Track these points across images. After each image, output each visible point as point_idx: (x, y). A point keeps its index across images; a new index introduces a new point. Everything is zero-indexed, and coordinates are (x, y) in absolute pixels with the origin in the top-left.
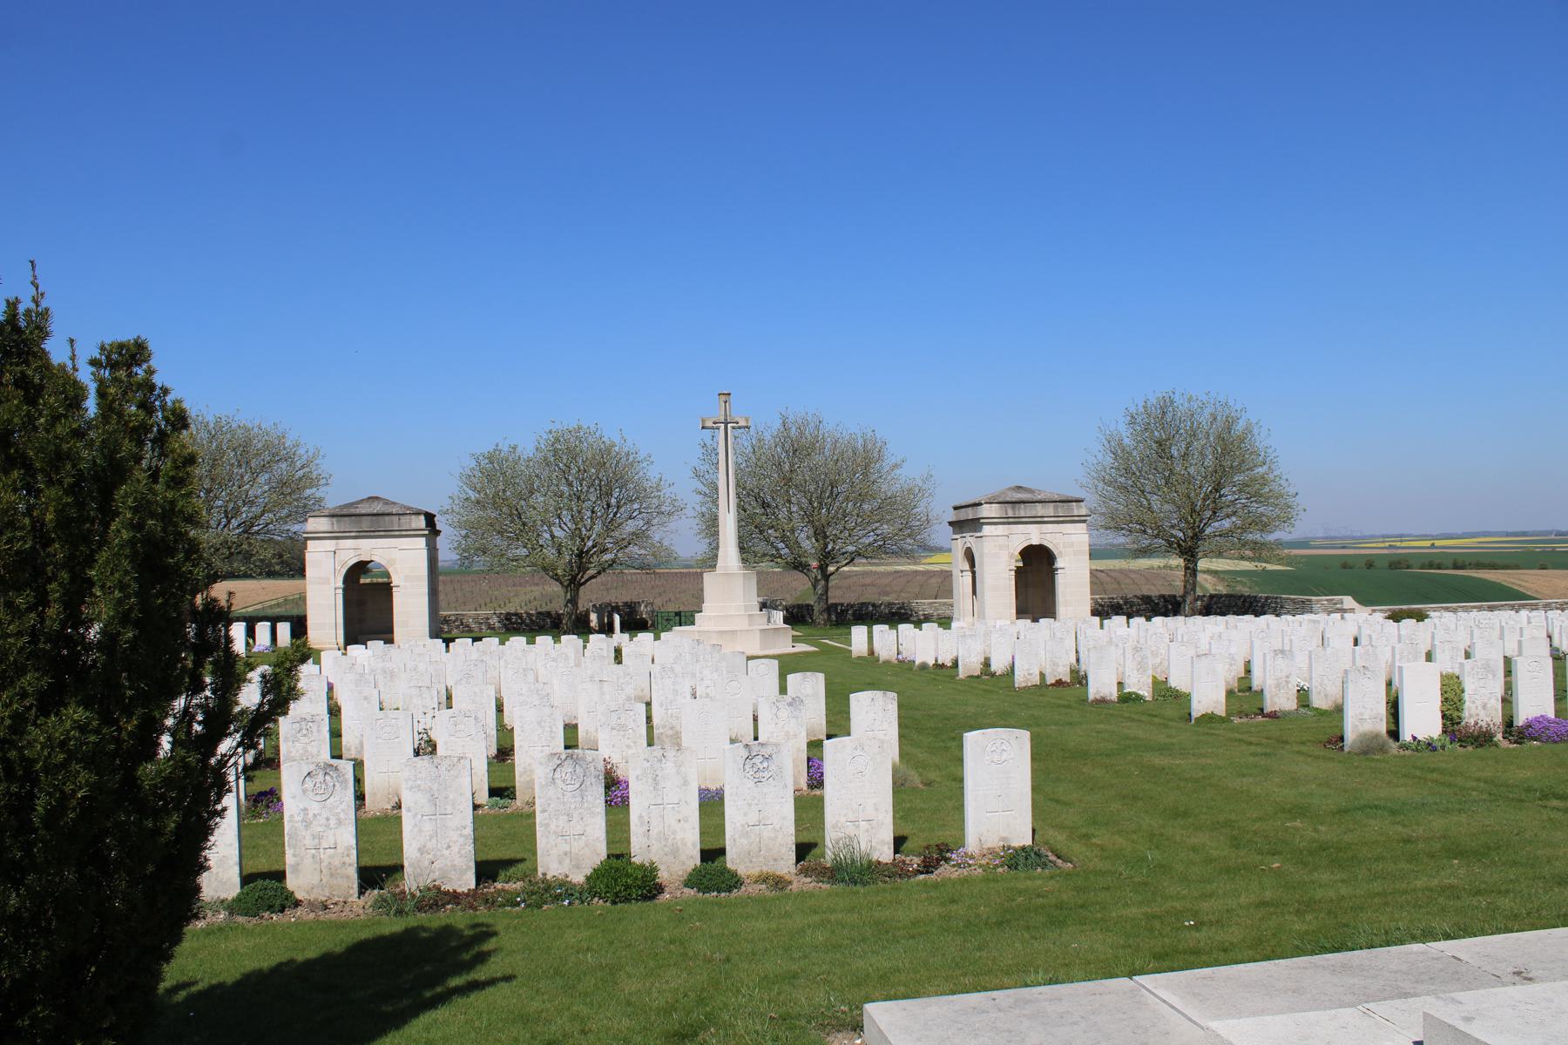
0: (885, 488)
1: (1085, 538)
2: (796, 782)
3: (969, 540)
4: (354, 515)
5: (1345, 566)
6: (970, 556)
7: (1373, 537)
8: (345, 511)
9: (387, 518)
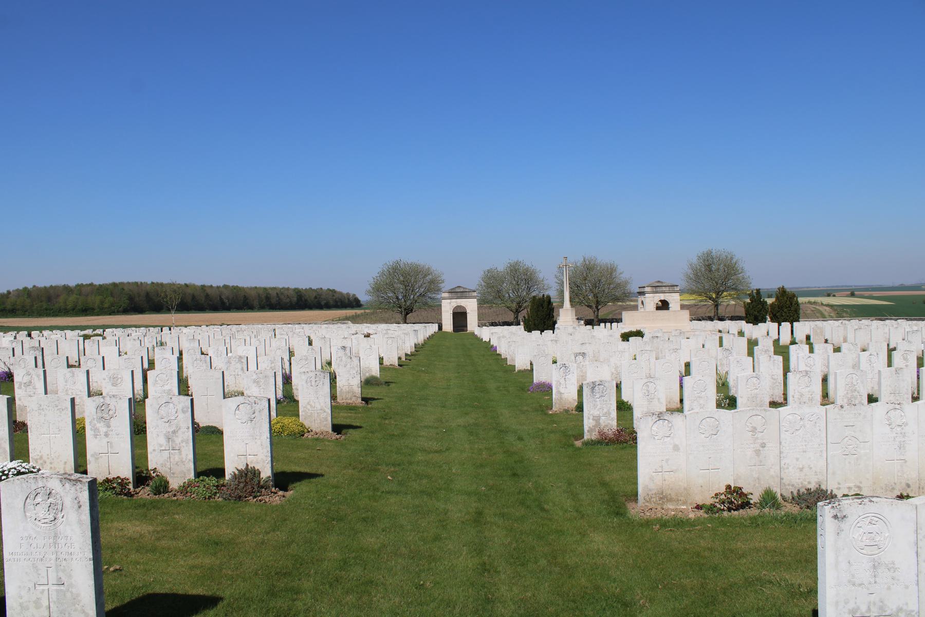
8: (453, 291)
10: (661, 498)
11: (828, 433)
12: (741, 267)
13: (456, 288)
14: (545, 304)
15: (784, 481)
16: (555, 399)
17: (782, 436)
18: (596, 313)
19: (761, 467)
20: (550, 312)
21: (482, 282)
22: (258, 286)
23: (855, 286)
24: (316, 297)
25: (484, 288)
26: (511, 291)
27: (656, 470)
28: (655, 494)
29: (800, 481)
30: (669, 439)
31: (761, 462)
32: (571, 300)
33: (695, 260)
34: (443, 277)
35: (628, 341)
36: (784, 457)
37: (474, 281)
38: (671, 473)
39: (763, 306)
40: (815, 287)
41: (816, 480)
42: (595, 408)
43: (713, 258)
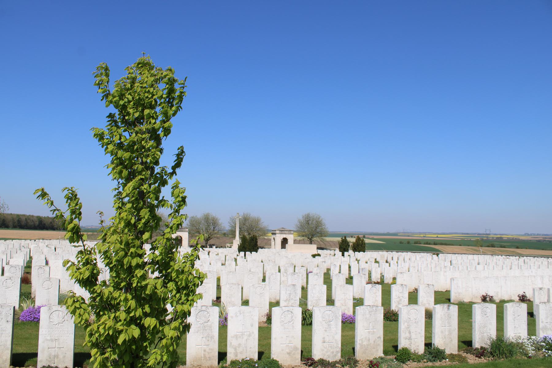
0: (260, 226)
1: (293, 237)
2: (299, 296)
3: (274, 236)
5: (401, 243)
6: (274, 239)
7: (416, 233)
22: (13, 213)
23: (364, 232)
24: (51, 223)
33: (301, 218)
35: (315, 258)
40: (343, 232)
43: (310, 217)
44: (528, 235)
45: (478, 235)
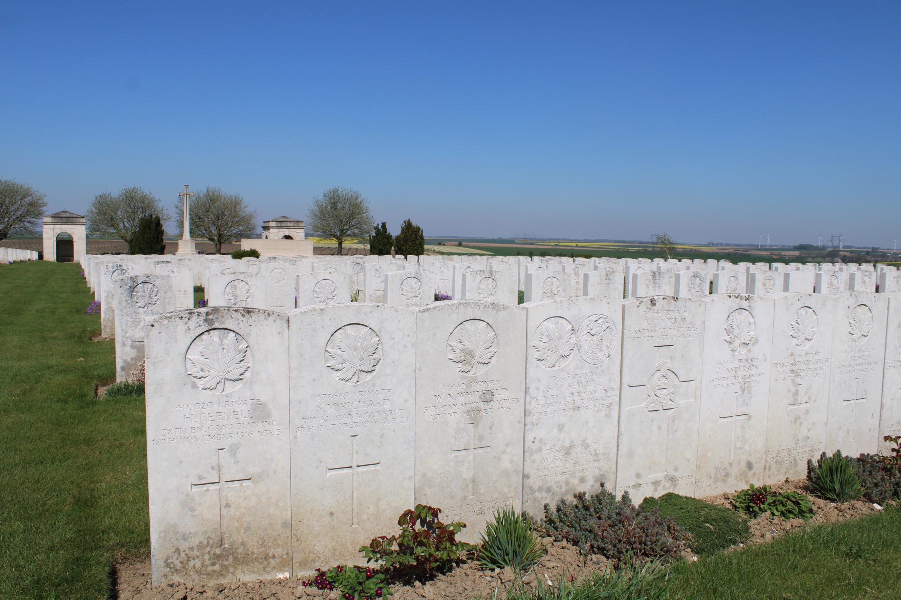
4: (60, 217)
7: (544, 240)
9: (72, 219)
10: (218, 557)
11: (626, 362)
12: (366, 207)
13: (61, 212)
14: (153, 226)
15: (530, 482)
16: (104, 320)
17: (531, 373)
18: (218, 247)
19: (480, 451)
20: (158, 235)
21: (93, 208)
23: (462, 238)
25: (96, 215)
26: (126, 220)
27: (200, 478)
28: (200, 547)
29: (563, 477)
30: (239, 385)
31: (481, 438)
32: (192, 233)
33: (321, 197)
34: (46, 200)
36: (533, 424)
37: (83, 206)
38: (245, 484)
39: (388, 240)
41: (596, 472)
42: (136, 327)
44: (713, 245)
45: (638, 244)
